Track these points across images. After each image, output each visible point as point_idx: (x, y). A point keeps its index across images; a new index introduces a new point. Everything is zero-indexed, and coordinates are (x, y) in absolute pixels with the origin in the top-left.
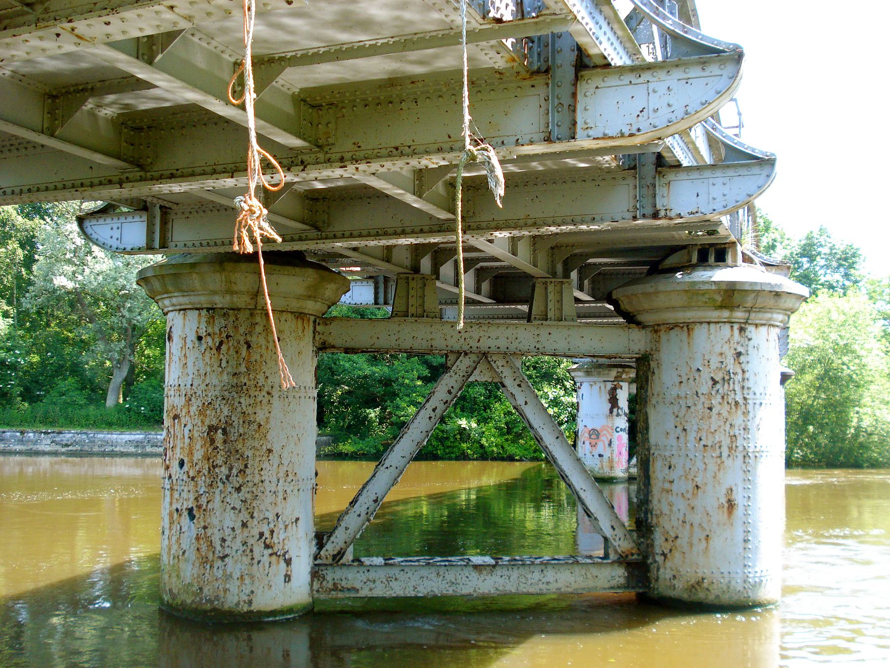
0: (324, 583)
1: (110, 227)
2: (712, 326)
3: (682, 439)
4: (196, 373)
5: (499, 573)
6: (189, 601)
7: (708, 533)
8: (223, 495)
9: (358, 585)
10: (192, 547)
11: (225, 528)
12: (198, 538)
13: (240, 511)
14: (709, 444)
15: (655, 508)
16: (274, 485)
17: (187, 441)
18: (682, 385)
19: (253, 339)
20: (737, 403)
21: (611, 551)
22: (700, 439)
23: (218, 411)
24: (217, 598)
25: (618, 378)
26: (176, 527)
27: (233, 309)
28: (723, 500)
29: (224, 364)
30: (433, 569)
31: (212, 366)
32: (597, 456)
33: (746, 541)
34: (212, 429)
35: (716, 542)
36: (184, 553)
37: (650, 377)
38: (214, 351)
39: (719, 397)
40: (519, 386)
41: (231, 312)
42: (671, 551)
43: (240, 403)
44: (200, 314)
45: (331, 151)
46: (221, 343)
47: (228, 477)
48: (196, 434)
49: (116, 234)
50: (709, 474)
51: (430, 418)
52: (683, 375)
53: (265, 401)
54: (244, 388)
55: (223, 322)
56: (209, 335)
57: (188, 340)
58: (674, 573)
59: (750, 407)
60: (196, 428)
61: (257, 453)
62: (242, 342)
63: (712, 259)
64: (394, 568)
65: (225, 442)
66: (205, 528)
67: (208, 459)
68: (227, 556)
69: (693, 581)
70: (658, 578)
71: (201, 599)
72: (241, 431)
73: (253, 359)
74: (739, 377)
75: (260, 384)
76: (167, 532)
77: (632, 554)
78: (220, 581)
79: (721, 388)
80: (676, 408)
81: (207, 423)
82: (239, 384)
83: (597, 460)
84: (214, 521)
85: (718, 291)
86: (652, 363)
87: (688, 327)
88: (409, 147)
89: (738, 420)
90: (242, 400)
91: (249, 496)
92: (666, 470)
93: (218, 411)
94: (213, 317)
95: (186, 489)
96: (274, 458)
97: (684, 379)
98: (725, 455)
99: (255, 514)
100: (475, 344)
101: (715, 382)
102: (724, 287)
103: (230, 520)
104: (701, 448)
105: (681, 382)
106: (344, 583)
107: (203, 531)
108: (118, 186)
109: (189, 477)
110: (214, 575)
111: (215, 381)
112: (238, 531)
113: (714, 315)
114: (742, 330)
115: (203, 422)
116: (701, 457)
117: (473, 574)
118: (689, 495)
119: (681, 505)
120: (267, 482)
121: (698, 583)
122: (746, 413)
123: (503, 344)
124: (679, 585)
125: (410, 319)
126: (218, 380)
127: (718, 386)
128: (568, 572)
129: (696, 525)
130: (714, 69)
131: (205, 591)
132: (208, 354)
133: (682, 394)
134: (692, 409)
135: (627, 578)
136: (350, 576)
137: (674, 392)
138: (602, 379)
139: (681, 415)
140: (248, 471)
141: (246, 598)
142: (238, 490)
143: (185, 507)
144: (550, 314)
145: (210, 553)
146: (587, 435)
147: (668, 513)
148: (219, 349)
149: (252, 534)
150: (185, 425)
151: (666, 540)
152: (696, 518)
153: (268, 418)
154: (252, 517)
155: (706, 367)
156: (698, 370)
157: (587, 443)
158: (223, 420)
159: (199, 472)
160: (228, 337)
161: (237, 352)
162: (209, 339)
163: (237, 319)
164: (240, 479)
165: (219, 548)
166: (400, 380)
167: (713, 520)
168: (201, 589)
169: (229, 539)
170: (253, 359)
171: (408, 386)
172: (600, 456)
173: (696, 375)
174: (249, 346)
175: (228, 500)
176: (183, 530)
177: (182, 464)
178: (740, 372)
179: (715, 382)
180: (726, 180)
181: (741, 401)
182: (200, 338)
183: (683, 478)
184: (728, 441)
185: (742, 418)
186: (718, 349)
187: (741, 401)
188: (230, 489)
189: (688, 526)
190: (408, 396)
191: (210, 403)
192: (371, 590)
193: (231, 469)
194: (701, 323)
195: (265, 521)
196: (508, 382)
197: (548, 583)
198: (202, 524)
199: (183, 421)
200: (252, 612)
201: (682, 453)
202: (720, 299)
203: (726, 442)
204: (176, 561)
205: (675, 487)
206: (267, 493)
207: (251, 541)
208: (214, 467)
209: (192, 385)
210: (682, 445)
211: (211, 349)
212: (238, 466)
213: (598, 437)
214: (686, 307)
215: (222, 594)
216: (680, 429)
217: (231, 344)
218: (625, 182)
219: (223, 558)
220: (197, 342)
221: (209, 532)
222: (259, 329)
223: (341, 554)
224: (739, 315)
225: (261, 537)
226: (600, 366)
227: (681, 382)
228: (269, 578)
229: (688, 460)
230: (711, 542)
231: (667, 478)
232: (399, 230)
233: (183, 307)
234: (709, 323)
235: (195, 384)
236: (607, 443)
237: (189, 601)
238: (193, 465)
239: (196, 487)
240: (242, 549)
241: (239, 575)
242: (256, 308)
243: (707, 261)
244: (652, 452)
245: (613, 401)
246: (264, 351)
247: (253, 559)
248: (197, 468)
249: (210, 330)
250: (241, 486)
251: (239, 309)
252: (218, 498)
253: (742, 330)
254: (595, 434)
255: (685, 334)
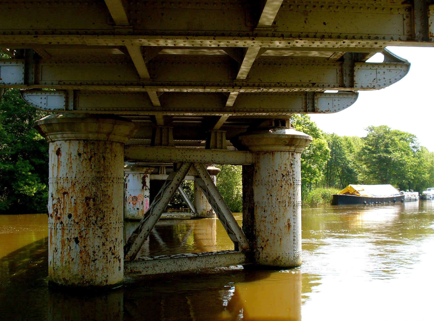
0: (127, 270)
1: (40, 97)
2: (282, 153)
3: (270, 200)
4: (78, 171)
5: (198, 260)
6: (76, 283)
7: (281, 237)
8: (94, 231)
9: (141, 270)
10: (78, 257)
11: (95, 246)
12: (81, 252)
13: (102, 238)
14: (281, 201)
15: (257, 228)
16: (115, 224)
17: (73, 204)
18: (270, 177)
19: (106, 155)
20: (291, 184)
21: (239, 248)
22: (278, 199)
23: (91, 190)
24: (92, 280)
25: (146, 172)
26: (67, 248)
27: (97, 140)
28: (286, 224)
29: (93, 167)
30: (172, 260)
31: (86, 168)
32: (136, 209)
33: (294, 240)
34: (87, 199)
35: (284, 241)
36: (73, 260)
37: (254, 174)
38: (88, 161)
39: (285, 182)
40: (205, 177)
41: (96, 142)
42: (265, 246)
43: (101, 186)
44: (79, 143)
45: (249, 81)
46: (91, 157)
47: (96, 222)
48: (79, 201)
49: (44, 101)
50: (281, 214)
51: (170, 192)
52: (270, 172)
53: (111, 185)
54: (103, 179)
55: (92, 147)
56: (85, 153)
57: (73, 155)
58: (267, 255)
59: (295, 186)
60: (79, 198)
61: (109, 210)
62: (101, 157)
63: (280, 125)
64: (156, 261)
65: (94, 205)
66: (85, 247)
67: (86, 213)
68: (96, 259)
69: (275, 258)
70: (259, 257)
71: (84, 281)
72: (102, 199)
73: (106, 165)
74: (292, 174)
75: (109, 177)
76: (60, 251)
77: (247, 249)
78: (93, 272)
79: (286, 178)
80: (267, 186)
81: (85, 195)
82: (100, 177)
83: (136, 211)
84: (90, 243)
85: (288, 139)
86: (256, 168)
87: (273, 153)
88: (284, 83)
89: (291, 192)
90: (102, 185)
91: (105, 230)
92: (263, 212)
93: (91, 190)
94: (87, 144)
95: (73, 228)
96: (115, 212)
97: (271, 174)
98: (287, 205)
99: (108, 239)
100: (188, 159)
101: (283, 176)
102: (291, 137)
103: (98, 242)
104: (278, 203)
105: (270, 176)
106: (135, 270)
107: (84, 249)
108: (142, 87)
109: (75, 222)
110: (90, 269)
111: (89, 175)
112: (101, 247)
113: (284, 148)
114: (292, 154)
115: (82, 195)
116: (278, 207)
117: (188, 261)
118: (273, 222)
119: (269, 226)
120: (112, 223)
121: (277, 258)
122: (294, 188)
123: (199, 158)
124: (270, 260)
125: (163, 147)
126: (90, 175)
127: (284, 177)
128: (224, 258)
129: (276, 234)
130: (399, 67)
131: (86, 277)
132: (84, 162)
133: (270, 181)
134: (274, 187)
135: (246, 259)
136: (138, 266)
137: (267, 180)
138: (139, 173)
139: (269, 189)
140: (105, 218)
141: (105, 279)
142: (101, 228)
143: (73, 237)
144: (218, 146)
145: (87, 259)
146: (131, 199)
147: (264, 230)
148: (90, 160)
149: (107, 248)
150: (72, 197)
151: (263, 241)
152: (276, 232)
153: (112, 193)
154: (107, 240)
155: (280, 170)
156: (277, 171)
157: (131, 203)
158: (93, 194)
159: (81, 220)
160: (95, 154)
161: (99, 161)
162: (85, 155)
163: (99, 145)
164: (101, 222)
165: (92, 256)
166: (20, 172)
167: (283, 232)
168: (83, 277)
169: (97, 251)
170: (106, 165)
171: (24, 175)
172: (138, 209)
173: (276, 173)
174: (104, 159)
175: (96, 233)
176: (72, 248)
177: (70, 216)
178: (292, 171)
179: (283, 176)
180: (339, 99)
181: (292, 183)
182: (80, 155)
183: (271, 215)
184: (288, 200)
185: (293, 190)
186: (284, 162)
187: (292, 183)
188: (97, 228)
189: (273, 235)
190: (23, 180)
191: (86, 186)
192: (147, 271)
193: (97, 218)
194: (278, 151)
195: (112, 242)
196: (201, 175)
197: (217, 263)
198: (83, 245)
199: (70, 195)
200: (107, 285)
201: (270, 205)
202: (288, 142)
203: (287, 200)
204: (67, 264)
205: (267, 219)
206: (113, 228)
207: (107, 252)
208: (89, 217)
209: (75, 177)
210: (270, 202)
211: (86, 160)
212: (101, 216)
213: (137, 200)
214: (274, 145)
215: (94, 278)
216: (269, 195)
217: (96, 157)
218: (301, 97)
219: (94, 261)
220: (78, 157)
221: (87, 249)
222: (108, 150)
223: (134, 255)
224: (293, 148)
225: (110, 250)
226: (139, 166)
227: (270, 176)
228: (114, 269)
229: (273, 208)
230: (282, 241)
231: (263, 215)
232: (202, 109)
233: (70, 139)
234: (281, 151)
235: (78, 177)
236: (141, 203)
237: (76, 283)
238: (77, 216)
239: (79, 227)
240: (103, 256)
241: (101, 268)
242: (107, 141)
243: (285, 126)
244: (255, 205)
245: (144, 183)
246: (110, 161)
247: (107, 260)
248: (80, 218)
249: (85, 150)
250: (102, 226)
251: (100, 141)
252: (91, 232)
253: (292, 154)
254: (135, 198)
255: (271, 156)
